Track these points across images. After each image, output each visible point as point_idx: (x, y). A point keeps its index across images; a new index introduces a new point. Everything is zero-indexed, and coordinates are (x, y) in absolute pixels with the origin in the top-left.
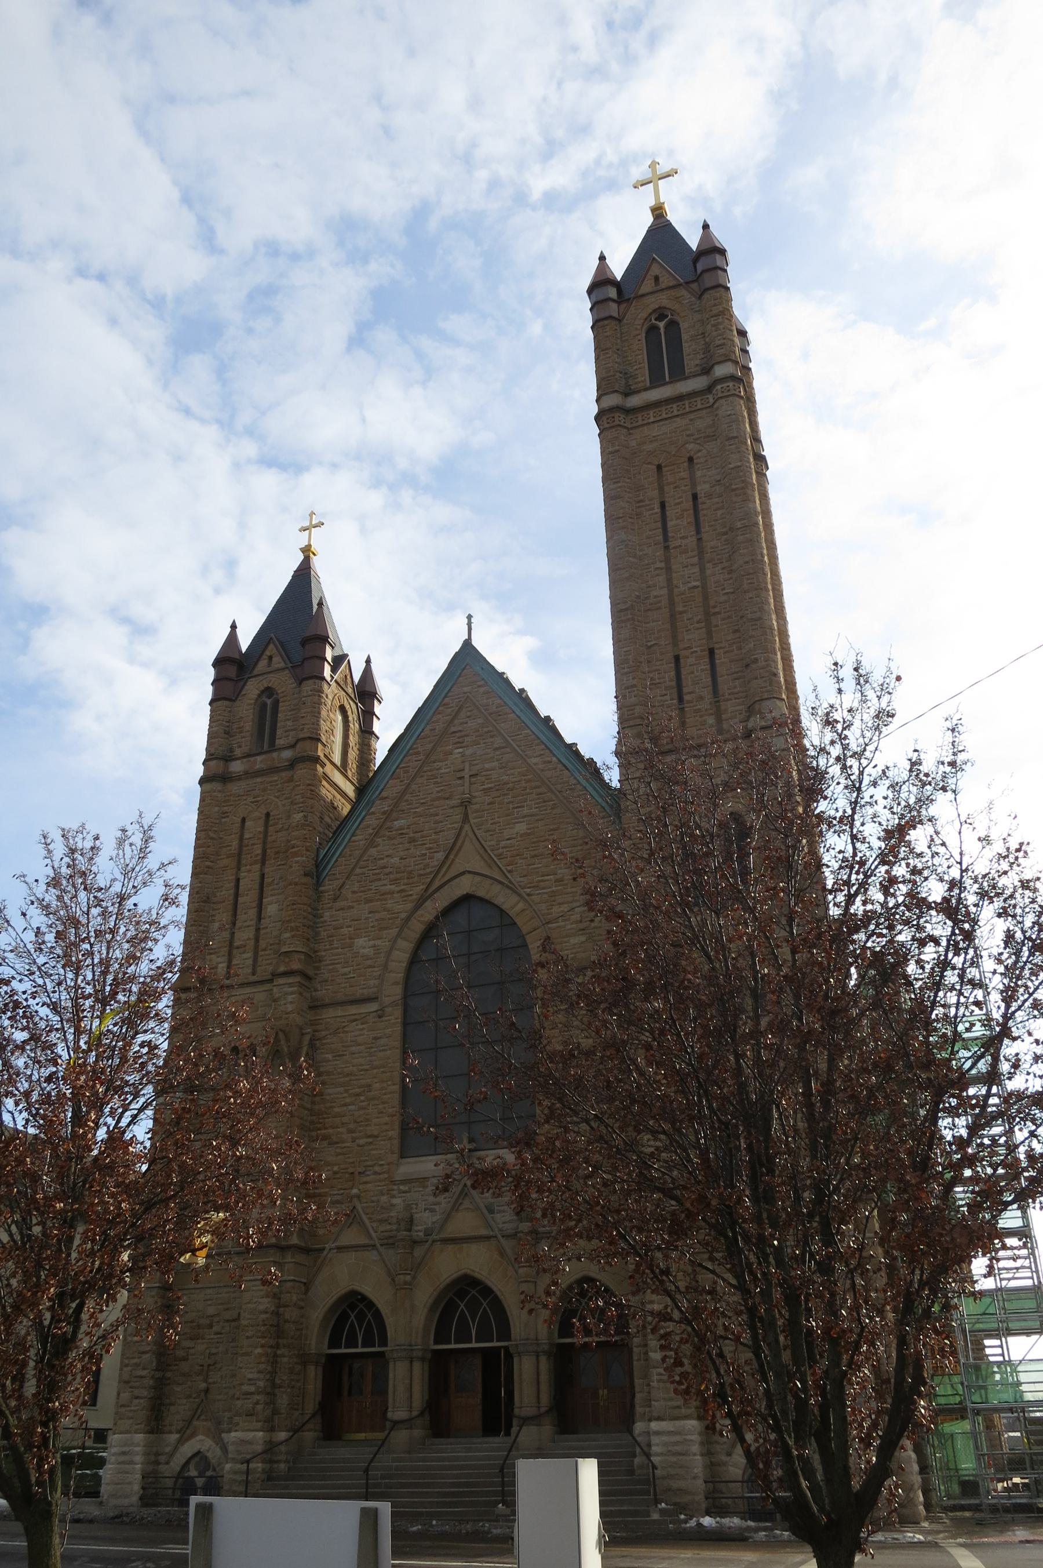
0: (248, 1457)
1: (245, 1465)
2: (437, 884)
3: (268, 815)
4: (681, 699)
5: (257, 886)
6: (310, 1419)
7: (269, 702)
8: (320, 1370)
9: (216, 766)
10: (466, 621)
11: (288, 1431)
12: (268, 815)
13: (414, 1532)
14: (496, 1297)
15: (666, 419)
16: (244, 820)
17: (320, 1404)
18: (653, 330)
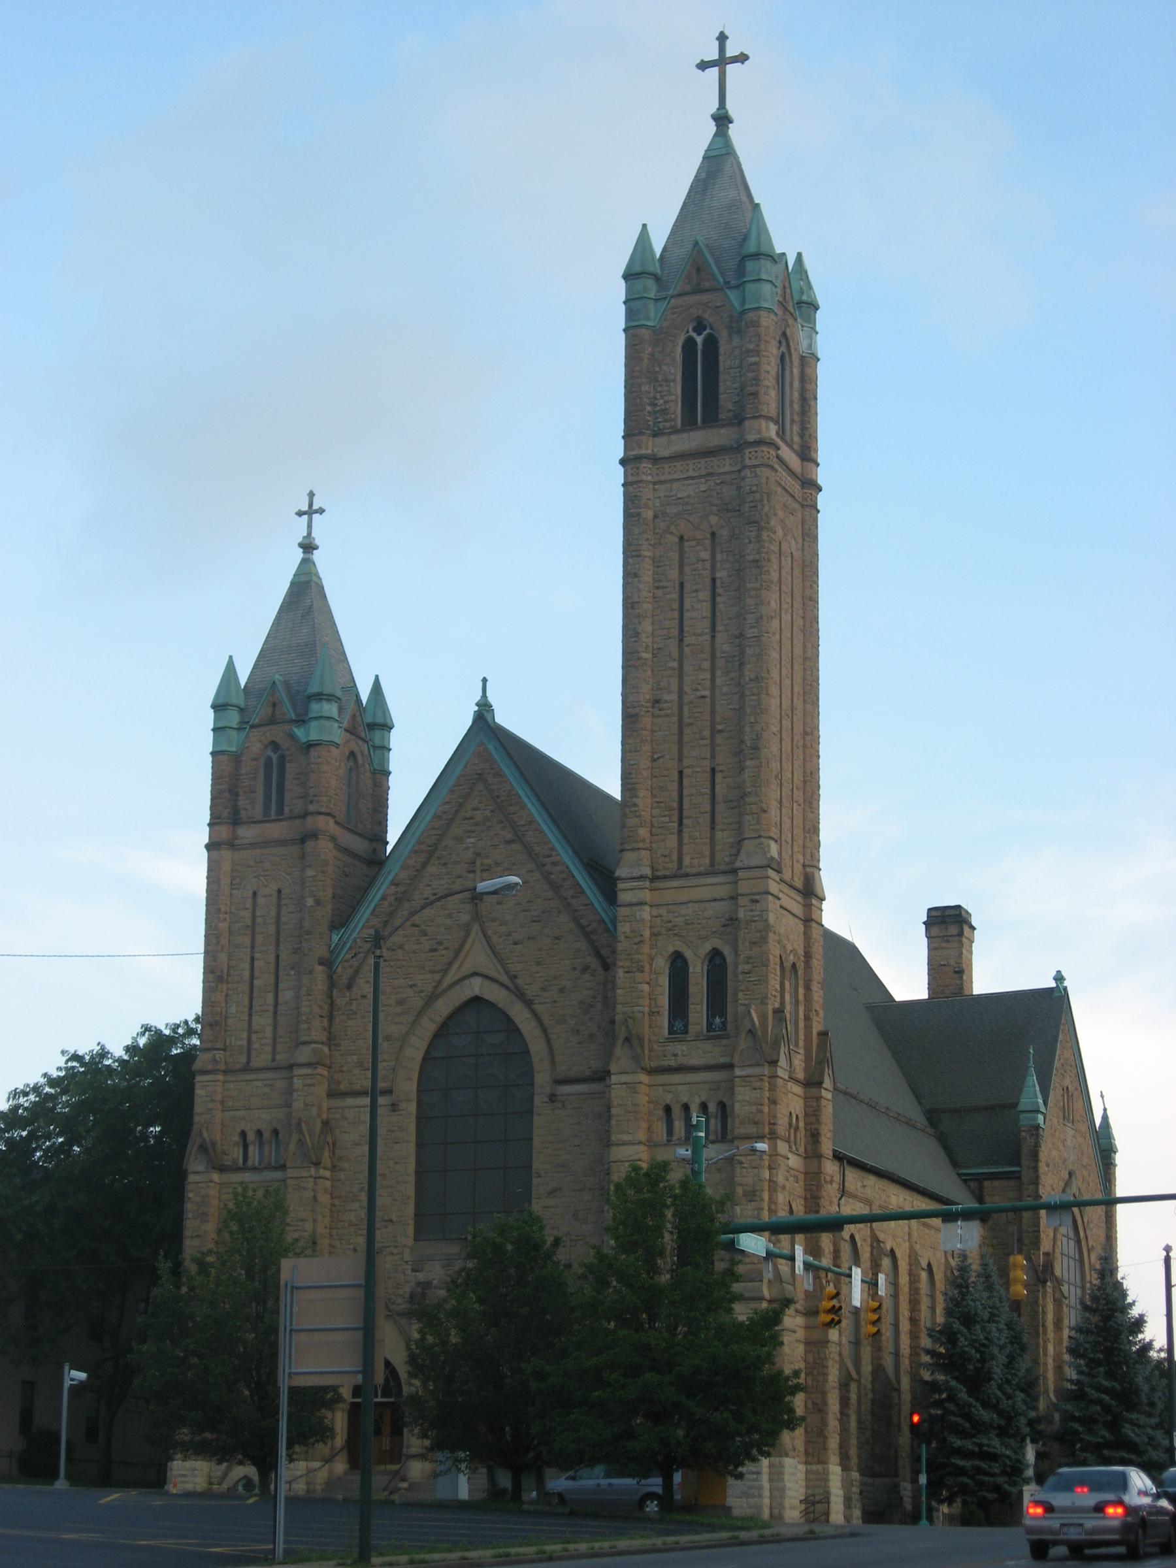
0: (290, 1479)
1: (288, 1485)
2: (448, 981)
3: (279, 891)
4: (681, 824)
5: (272, 968)
6: (339, 1452)
7: (274, 757)
8: (346, 1415)
9: (224, 832)
10: (481, 684)
11: (321, 1461)
12: (279, 891)
13: (78, 1062)
14: (394, 1368)
15: (692, 478)
16: (255, 894)
17: (346, 1441)
18: (689, 344)
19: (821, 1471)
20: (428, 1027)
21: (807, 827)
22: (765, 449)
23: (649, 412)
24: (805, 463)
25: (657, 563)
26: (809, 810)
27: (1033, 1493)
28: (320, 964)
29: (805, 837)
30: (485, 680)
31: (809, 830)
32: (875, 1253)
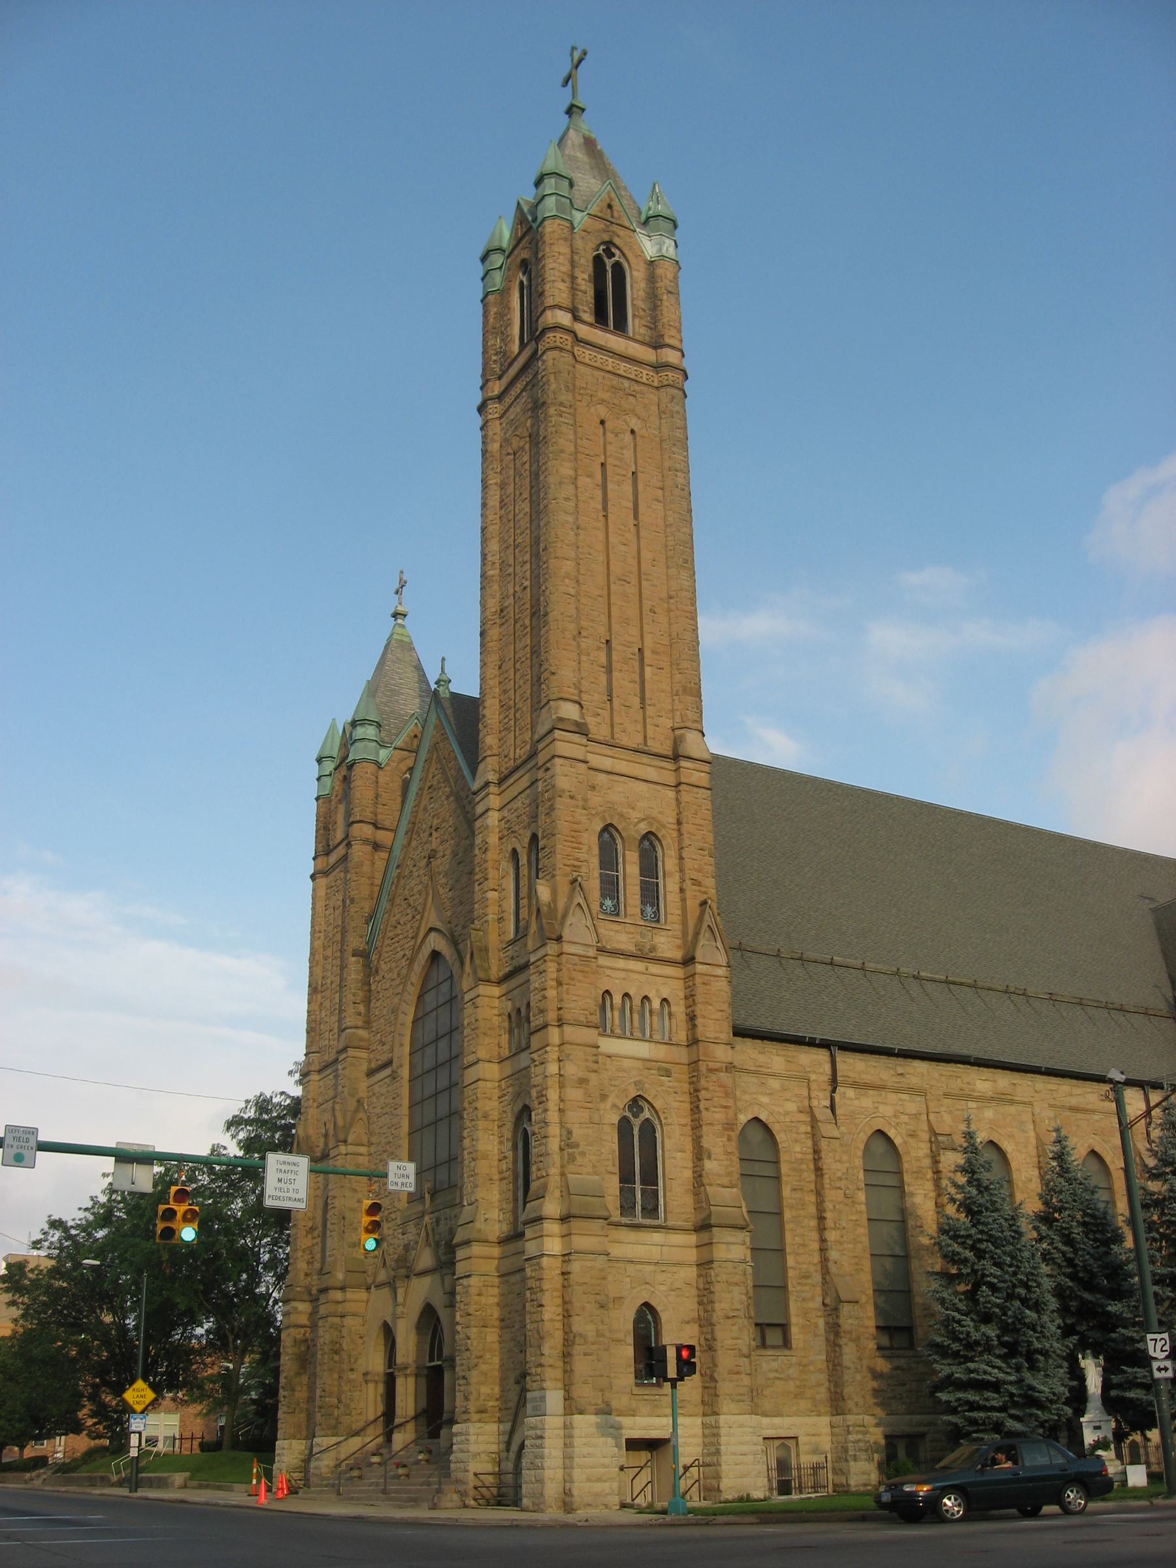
19: (713, 1423)
20: (413, 991)
21: (675, 689)
22: (551, 335)
23: (495, 361)
24: (659, 351)
25: (502, 486)
26: (677, 672)
27: (1097, 1424)
28: (353, 955)
29: (673, 700)
30: (443, 659)
31: (677, 691)
32: (934, 1149)
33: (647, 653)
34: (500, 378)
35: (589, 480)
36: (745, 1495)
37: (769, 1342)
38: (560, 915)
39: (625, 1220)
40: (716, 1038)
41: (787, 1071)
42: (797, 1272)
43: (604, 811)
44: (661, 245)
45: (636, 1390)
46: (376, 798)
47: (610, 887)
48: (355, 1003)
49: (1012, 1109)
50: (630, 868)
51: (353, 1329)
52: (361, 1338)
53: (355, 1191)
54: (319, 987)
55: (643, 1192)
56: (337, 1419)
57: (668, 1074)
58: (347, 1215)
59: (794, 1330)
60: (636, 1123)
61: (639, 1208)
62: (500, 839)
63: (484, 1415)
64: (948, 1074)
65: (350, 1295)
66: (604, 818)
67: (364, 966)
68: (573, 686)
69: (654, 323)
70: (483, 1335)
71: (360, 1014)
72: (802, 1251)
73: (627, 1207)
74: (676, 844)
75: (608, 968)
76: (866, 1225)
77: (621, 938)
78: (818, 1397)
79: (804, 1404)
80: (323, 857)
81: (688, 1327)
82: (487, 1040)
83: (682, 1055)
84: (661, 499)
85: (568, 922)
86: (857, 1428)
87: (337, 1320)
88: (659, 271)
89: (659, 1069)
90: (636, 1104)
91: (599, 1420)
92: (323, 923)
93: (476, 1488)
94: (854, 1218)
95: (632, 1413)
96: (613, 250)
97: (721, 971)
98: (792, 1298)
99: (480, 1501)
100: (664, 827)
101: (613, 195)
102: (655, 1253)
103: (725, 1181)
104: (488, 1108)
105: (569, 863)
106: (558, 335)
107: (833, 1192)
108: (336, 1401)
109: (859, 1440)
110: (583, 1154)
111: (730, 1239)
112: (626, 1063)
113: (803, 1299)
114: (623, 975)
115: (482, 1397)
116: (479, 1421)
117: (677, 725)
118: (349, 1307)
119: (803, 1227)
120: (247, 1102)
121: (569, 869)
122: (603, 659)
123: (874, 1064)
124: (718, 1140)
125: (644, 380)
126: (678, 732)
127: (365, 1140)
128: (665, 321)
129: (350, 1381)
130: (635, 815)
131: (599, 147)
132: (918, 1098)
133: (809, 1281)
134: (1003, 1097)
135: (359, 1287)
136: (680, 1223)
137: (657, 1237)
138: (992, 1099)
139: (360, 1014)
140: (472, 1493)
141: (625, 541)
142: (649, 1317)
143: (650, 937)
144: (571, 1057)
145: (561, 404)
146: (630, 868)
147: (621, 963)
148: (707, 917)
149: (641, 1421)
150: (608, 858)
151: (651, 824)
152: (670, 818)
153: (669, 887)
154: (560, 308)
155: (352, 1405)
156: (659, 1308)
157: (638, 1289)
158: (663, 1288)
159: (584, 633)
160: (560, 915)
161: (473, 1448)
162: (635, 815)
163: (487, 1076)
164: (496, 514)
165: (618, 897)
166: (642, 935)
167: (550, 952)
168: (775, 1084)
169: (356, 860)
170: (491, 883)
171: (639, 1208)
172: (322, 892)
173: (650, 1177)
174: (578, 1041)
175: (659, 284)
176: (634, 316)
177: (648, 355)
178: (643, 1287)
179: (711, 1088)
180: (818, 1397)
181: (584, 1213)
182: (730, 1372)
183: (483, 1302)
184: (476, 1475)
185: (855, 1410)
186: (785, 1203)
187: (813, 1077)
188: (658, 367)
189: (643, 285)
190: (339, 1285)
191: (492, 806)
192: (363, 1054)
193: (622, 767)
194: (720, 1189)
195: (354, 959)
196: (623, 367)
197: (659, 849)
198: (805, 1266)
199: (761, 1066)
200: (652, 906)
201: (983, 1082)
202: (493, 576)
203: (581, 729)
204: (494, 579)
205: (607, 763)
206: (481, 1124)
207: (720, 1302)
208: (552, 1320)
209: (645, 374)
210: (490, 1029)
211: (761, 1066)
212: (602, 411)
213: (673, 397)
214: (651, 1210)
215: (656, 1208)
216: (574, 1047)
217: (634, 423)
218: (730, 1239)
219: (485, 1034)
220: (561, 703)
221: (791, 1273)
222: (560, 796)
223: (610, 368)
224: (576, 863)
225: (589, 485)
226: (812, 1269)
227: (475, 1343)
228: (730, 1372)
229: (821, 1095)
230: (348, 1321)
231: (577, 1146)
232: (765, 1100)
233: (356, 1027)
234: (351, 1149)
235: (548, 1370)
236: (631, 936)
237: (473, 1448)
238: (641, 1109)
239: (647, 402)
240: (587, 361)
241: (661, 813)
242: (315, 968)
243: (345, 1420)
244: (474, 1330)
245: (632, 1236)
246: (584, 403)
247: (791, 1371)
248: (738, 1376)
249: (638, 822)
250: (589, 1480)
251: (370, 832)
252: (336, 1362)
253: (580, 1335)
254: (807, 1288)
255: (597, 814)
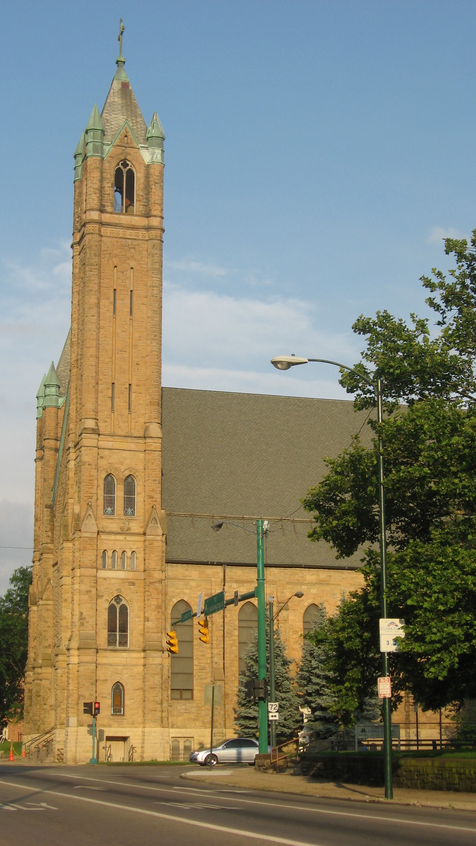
23: (78, 221)
28: (46, 507)
33: (134, 387)
34: (79, 232)
35: (106, 301)
36: (154, 760)
37: (184, 697)
38: (82, 519)
39: (111, 648)
40: (154, 568)
41: (199, 578)
42: (198, 667)
43: (108, 468)
44: (153, 154)
45: (112, 717)
46: (57, 425)
47: (110, 502)
48: (46, 531)
49: (328, 588)
50: (119, 493)
51: (45, 686)
52: (49, 690)
53: (46, 622)
54: (39, 519)
55: (120, 636)
56: (39, 726)
57: (133, 584)
58: (43, 634)
59: (195, 692)
60: (118, 607)
61: (118, 642)
62: (74, 474)
63: (63, 726)
64: (290, 573)
65: (44, 670)
66: (107, 471)
67: (51, 512)
68: (92, 411)
69: (147, 205)
70: (63, 693)
71: (49, 536)
72: (202, 658)
73: (111, 642)
74: (143, 479)
75: (105, 539)
76: (238, 645)
77: (114, 526)
78: (206, 720)
79: (198, 724)
80: (39, 451)
81: (137, 692)
82: (67, 568)
83: (142, 576)
84: (146, 303)
85: (84, 523)
86: (219, 734)
87: (38, 682)
88: (152, 171)
89: (129, 582)
90: (118, 598)
91: (89, 729)
92: (40, 485)
93: (58, 755)
94: (231, 642)
95: (110, 726)
96: (128, 162)
97: (159, 538)
98: (195, 678)
99: (60, 760)
100: (137, 471)
101: (128, 129)
102: (124, 661)
103: (155, 630)
104: (66, 597)
105: (87, 495)
106: (91, 226)
107: (217, 632)
108: (39, 718)
109: (219, 739)
110: (88, 622)
111: (155, 655)
112: (113, 581)
113: (201, 679)
114: (113, 542)
115: (62, 719)
116: (61, 728)
117: (147, 421)
118: (43, 676)
119: (203, 647)
120: (16, 571)
121: (86, 498)
122: (110, 394)
123: (247, 571)
124: (153, 613)
125: (140, 238)
126: (147, 424)
127: (51, 597)
128: (152, 201)
129: (44, 709)
130: (123, 468)
131: (130, 88)
132: (272, 586)
133: (204, 671)
134: (322, 582)
135: (48, 666)
136: (136, 648)
137: (125, 654)
138: (316, 583)
139: (49, 536)
140: (57, 757)
141: (124, 330)
142: (121, 687)
143: (127, 524)
144: (83, 582)
145: (92, 265)
146: (119, 493)
147: (113, 537)
148: (153, 513)
149: (112, 729)
150: (109, 488)
151: (131, 471)
152: (141, 467)
153: (139, 499)
154: (93, 210)
155: (45, 720)
156: (124, 684)
157: (114, 676)
158: (126, 676)
159: (100, 382)
160: (82, 519)
161: (58, 739)
162: (123, 468)
163: (67, 583)
164: (76, 308)
165: (114, 506)
166: (124, 523)
167: (77, 536)
168: (193, 584)
169: (47, 458)
170: (70, 496)
171: (118, 642)
172: (39, 469)
173: (124, 629)
174: (87, 575)
175: (151, 179)
176: (137, 200)
177: (144, 222)
178: (117, 675)
179: (150, 591)
180: (206, 720)
181: (85, 647)
182: (152, 710)
183: (63, 679)
184: (58, 750)
185: (219, 726)
186: (194, 637)
187: (213, 579)
188: (148, 228)
189: (142, 180)
190: (39, 666)
191: (71, 458)
192: (51, 556)
193: (117, 445)
194: (153, 634)
195: (46, 509)
196: (129, 233)
197: (135, 481)
198: (203, 664)
199: (185, 576)
200: (131, 508)
201: (310, 575)
202: (74, 341)
203: (96, 432)
204: (75, 343)
205: (110, 445)
206: (64, 604)
207: (149, 681)
208: (73, 690)
209: (141, 234)
210: (68, 562)
211: (185, 576)
212: (116, 261)
213: (154, 246)
214: (123, 643)
215: (126, 642)
216: (84, 577)
217: (132, 264)
218: (155, 655)
219: (66, 564)
220: (86, 420)
221: (195, 668)
222: (84, 465)
223: (121, 235)
224: (90, 495)
225: (106, 304)
226: (206, 666)
227: (59, 697)
228: (152, 710)
229: (217, 587)
230: (43, 682)
231: (85, 619)
232: (187, 591)
233: (47, 543)
234: (45, 602)
235: (70, 709)
236: (118, 524)
237: (58, 739)
238: (121, 600)
239: (141, 249)
240: (108, 234)
241: (136, 465)
242: (36, 509)
243: (42, 727)
244: (59, 691)
245: (113, 654)
246: (106, 259)
247: (192, 709)
248: (155, 712)
249: (124, 471)
250: (83, 752)
251: (53, 444)
252: (38, 701)
253: (82, 696)
254: (203, 674)
255: (104, 469)
